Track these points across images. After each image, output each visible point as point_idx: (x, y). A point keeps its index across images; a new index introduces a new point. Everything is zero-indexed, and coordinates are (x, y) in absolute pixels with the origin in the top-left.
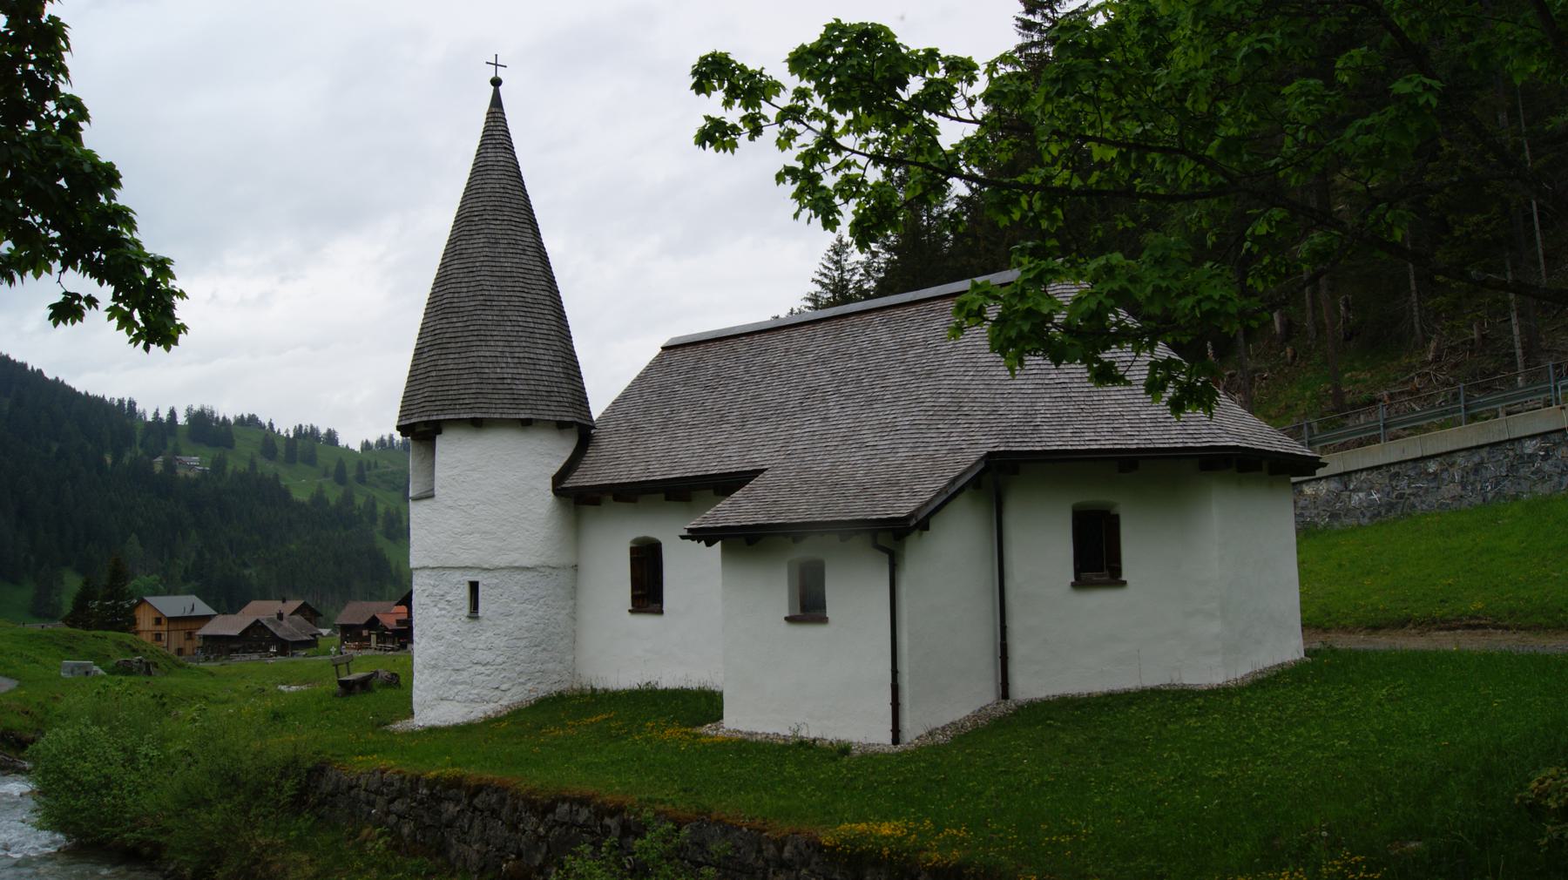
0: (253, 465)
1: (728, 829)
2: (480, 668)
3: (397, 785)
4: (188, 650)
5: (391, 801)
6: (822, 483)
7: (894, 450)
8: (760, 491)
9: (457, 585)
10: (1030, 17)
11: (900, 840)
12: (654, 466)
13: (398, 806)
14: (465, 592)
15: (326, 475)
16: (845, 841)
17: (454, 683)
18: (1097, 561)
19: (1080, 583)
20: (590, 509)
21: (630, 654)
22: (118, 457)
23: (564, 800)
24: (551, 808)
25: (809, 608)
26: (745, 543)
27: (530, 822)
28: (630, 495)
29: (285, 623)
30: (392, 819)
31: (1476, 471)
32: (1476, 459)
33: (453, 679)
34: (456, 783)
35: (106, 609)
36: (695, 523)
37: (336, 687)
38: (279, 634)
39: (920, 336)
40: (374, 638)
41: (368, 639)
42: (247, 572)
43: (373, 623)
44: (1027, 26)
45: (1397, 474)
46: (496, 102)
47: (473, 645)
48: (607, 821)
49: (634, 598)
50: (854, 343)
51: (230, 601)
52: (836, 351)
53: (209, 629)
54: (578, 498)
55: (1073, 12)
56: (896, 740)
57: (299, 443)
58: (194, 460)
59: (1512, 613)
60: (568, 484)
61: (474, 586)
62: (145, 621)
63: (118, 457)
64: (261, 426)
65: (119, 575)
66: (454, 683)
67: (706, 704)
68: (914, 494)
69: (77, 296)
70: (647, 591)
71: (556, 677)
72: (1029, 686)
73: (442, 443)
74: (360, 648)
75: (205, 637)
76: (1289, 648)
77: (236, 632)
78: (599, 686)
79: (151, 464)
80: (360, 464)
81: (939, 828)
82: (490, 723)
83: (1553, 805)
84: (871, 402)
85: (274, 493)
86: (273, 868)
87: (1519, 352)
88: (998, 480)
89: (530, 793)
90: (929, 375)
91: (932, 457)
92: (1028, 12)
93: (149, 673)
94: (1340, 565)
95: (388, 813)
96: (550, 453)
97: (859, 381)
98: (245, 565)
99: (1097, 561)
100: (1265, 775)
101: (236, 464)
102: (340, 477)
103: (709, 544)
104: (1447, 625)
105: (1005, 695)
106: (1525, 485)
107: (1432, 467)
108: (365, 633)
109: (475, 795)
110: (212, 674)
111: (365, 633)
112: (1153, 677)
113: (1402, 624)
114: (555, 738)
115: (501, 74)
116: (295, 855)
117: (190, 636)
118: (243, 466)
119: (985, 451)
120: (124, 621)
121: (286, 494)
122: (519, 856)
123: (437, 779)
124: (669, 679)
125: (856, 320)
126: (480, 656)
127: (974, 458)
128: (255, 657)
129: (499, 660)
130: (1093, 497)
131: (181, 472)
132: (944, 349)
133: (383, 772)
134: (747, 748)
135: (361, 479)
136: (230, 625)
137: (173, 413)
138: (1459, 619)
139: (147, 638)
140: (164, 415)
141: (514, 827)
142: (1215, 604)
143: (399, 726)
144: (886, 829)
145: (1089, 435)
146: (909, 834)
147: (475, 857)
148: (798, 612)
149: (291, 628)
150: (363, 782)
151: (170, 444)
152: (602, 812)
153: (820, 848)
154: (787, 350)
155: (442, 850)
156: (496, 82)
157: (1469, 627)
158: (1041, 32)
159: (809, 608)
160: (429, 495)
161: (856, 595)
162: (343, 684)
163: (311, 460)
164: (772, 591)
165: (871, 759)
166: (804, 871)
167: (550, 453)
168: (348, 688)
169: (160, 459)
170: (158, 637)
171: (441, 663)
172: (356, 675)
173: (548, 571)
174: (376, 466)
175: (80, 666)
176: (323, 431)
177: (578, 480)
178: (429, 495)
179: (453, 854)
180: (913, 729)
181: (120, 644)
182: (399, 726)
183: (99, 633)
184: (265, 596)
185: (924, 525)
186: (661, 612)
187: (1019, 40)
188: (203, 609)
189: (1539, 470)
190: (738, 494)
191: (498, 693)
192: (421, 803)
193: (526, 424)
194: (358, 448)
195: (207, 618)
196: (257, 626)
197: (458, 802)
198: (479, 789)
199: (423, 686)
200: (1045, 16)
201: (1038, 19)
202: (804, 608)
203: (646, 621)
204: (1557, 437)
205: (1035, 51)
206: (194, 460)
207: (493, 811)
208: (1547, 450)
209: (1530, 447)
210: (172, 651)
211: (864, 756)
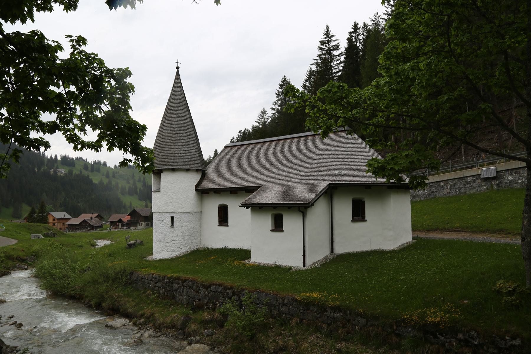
0: (81, 172)
1: (267, 294)
2: (174, 242)
3: (158, 278)
4: (63, 229)
5: (157, 283)
6: (280, 191)
7: (301, 182)
8: (261, 193)
10: (322, 46)
11: (320, 298)
12: (226, 183)
13: (158, 284)
14: (170, 219)
15: (103, 175)
16: (304, 299)
17: (166, 246)
18: (359, 214)
19: (354, 221)
21: (218, 238)
22: (39, 169)
23: (214, 285)
24: (210, 287)
25: (278, 226)
26: (257, 208)
27: (202, 291)
28: (218, 192)
29: (93, 220)
30: (157, 288)
31: (454, 185)
32: (454, 182)
33: (166, 244)
34: (178, 278)
35: (39, 217)
36: (243, 202)
37: (127, 246)
38: (91, 224)
39: (305, 147)
40: (120, 225)
41: (119, 225)
42: (79, 204)
43: (120, 221)
44: (321, 49)
45: (432, 186)
46: (178, 74)
48: (228, 291)
50: (285, 148)
51: (76, 215)
52: (279, 151)
53: (69, 222)
54: (202, 192)
55: (334, 46)
56: (304, 266)
57: (95, 165)
58: (63, 170)
60: (199, 188)
61: (172, 218)
62: (50, 220)
63: (39, 169)
64: (84, 160)
65: (43, 206)
66: (166, 246)
67: (246, 254)
68: (310, 196)
69: (127, 160)
70: (223, 220)
71: (196, 244)
72: (339, 250)
73: (163, 175)
74: (116, 228)
75: (69, 225)
76: (407, 238)
77: (78, 223)
78: (209, 247)
79: (50, 171)
80: (114, 172)
81: (330, 295)
82: (178, 258)
83: (505, 292)
84: (292, 166)
85: (88, 181)
86: (121, 303)
87: (463, 150)
88: (332, 191)
89: (203, 282)
90: (309, 159)
91: (312, 184)
92: (321, 45)
93: (54, 236)
94: (417, 212)
95: (155, 286)
96: (194, 179)
97: (288, 160)
98: (79, 202)
99: (359, 214)
100: (416, 278)
101: (76, 172)
102: (107, 176)
103: (247, 208)
104: (450, 230)
107: (442, 184)
108: (118, 224)
109: (184, 282)
110: (73, 237)
111: (118, 224)
112: (373, 248)
113: (436, 230)
114: (201, 264)
116: (127, 299)
117: (64, 224)
118: (78, 172)
119: (328, 183)
120: (44, 220)
121: (91, 181)
122: (199, 300)
123: (171, 277)
124: (231, 245)
125: (285, 141)
126: (174, 238)
127: (326, 185)
128: (84, 230)
129: (180, 239)
130: (357, 196)
131: (59, 174)
132: (313, 151)
133: (153, 274)
134: (260, 268)
135: (114, 176)
136: (76, 221)
137: (56, 156)
139: (51, 225)
140: (53, 157)
141: (197, 292)
142: (390, 226)
143: (149, 258)
144: (315, 295)
145: (358, 179)
146: (322, 297)
147: (185, 300)
148: (274, 229)
149: (95, 222)
150: (146, 277)
151: (55, 165)
152: (226, 288)
153: (296, 300)
154: (264, 149)
155: (174, 298)
156: (178, 68)
157: (455, 231)
158: (325, 51)
159: (278, 226)
160: (158, 190)
161: (292, 223)
162: (129, 245)
163: (98, 170)
164: (266, 221)
165: (298, 272)
166: (291, 307)
167: (194, 179)
168: (130, 246)
169: (52, 170)
170: (54, 224)
172: (132, 242)
174: (118, 173)
175: (37, 236)
176: (102, 162)
177: (202, 187)
178: (158, 190)
179: (177, 299)
180: (309, 262)
181: (45, 228)
183: (38, 224)
184: (85, 213)
185: (313, 205)
186: (228, 226)
187: (319, 53)
188: (69, 217)
189: (472, 186)
190: (255, 193)
192: (166, 284)
193: (188, 170)
194: (113, 167)
195: (69, 219)
196: (84, 221)
197: (178, 284)
198: (185, 280)
200: (326, 46)
201: (324, 47)
202: (276, 227)
204: (477, 177)
205: (324, 56)
206: (63, 170)
207: (190, 287)
208: (474, 180)
209: (469, 179)
210: (58, 229)
211: (296, 271)
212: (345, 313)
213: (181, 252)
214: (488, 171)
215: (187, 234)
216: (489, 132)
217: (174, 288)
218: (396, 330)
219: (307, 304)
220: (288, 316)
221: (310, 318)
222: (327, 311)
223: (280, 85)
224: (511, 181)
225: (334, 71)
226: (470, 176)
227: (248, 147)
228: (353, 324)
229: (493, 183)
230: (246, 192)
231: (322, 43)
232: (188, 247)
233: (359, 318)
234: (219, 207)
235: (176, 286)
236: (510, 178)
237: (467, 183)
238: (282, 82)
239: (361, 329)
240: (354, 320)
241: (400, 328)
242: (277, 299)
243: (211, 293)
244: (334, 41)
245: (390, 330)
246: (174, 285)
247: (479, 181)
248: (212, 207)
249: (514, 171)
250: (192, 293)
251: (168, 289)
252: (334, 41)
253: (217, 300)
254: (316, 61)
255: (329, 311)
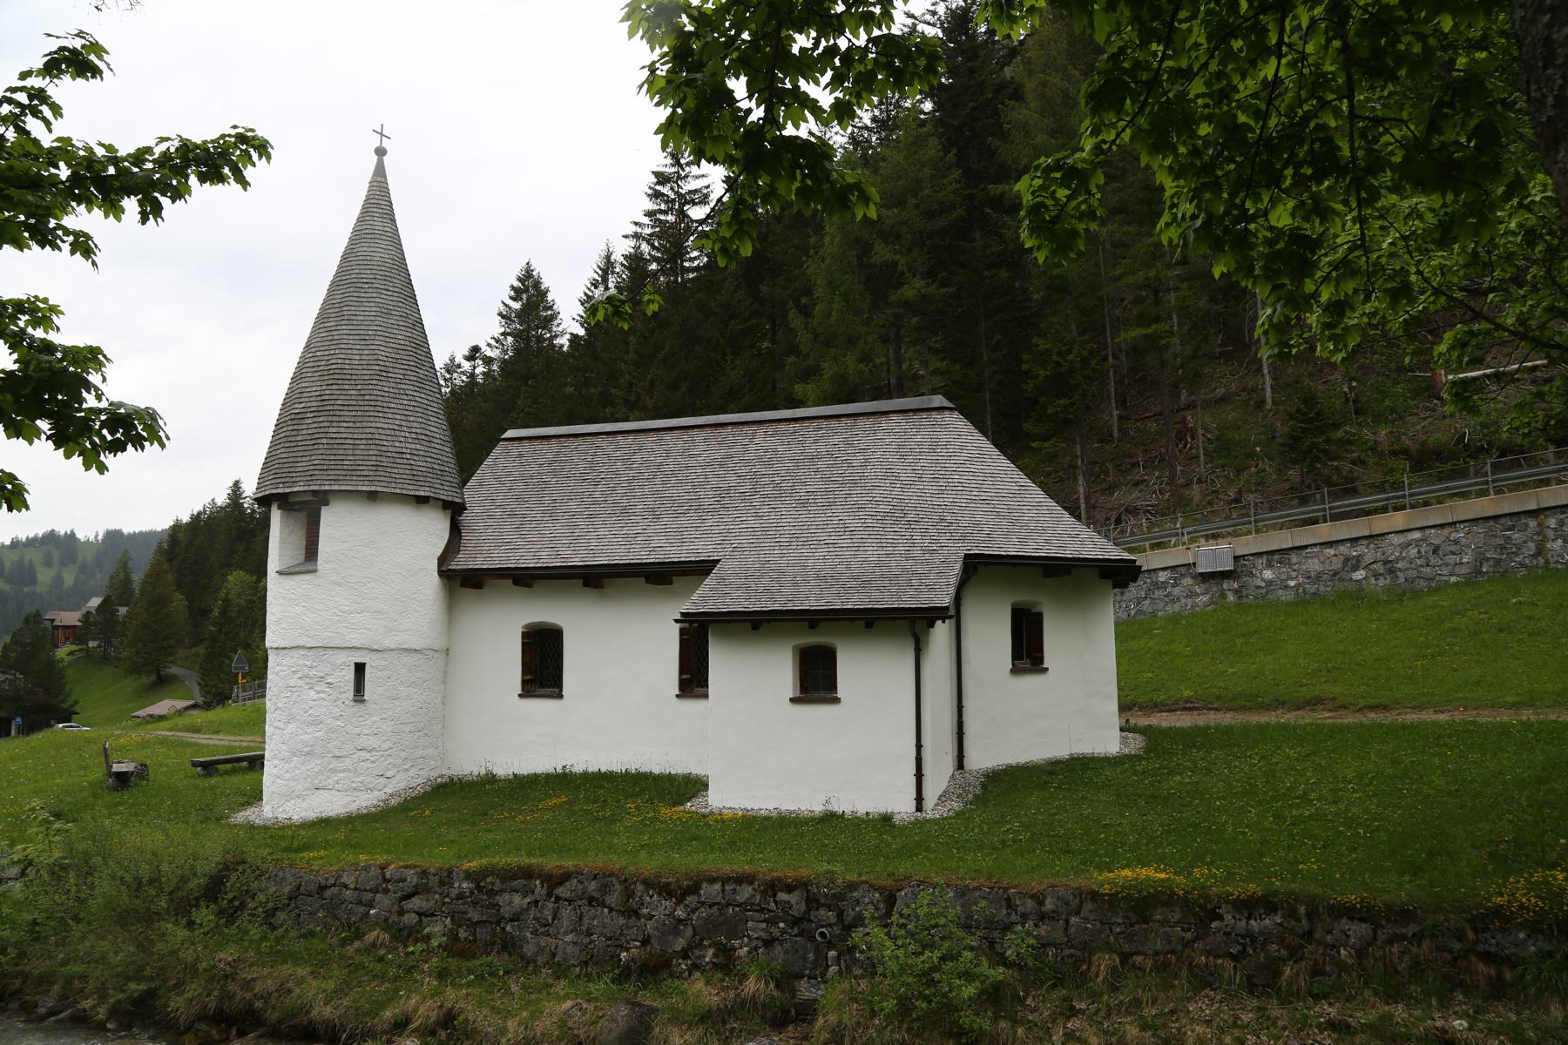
2: (363, 754)
9: (340, 667)
14: (350, 674)
16: (1124, 887)
17: (334, 771)
19: (1015, 671)
20: (470, 592)
21: (524, 740)
23: (712, 880)
24: (694, 889)
25: (817, 681)
27: (660, 908)
28: (525, 579)
46: (380, 171)
47: (358, 730)
48: (782, 896)
49: (524, 682)
54: (462, 581)
55: (696, 191)
56: (919, 808)
59: (1218, 698)
61: (360, 669)
66: (334, 771)
67: (695, 786)
72: (981, 758)
89: (658, 875)
92: (659, 183)
105: (960, 765)
106: (1160, 605)
109: (560, 883)
115: (386, 144)
122: (646, 942)
124: (585, 759)
129: (385, 746)
130: (1024, 597)
138: (1176, 702)
143: (241, 816)
155: (509, 946)
156: (381, 152)
157: (1186, 709)
158: (666, 202)
159: (817, 681)
161: (869, 673)
166: (1074, 920)
168: (122, 779)
171: (318, 750)
173: (431, 653)
177: (462, 562)
179: (529, 949)
182: (241, 816)
186: (560, 696)
187: (651, 206)
191: (382, 780)
199: (272, 776)
203: (540, 707)
204: (1183, 570)
209: (1163, 576)
212: (1292, 914)
213: (389, 790)
214: (1214, 554)
215: (408, 728)
216: (1133, 465)
217: (506, 911)
218: (1477, 942)
219: (1140, 905)
220: (1067, 952)
221: (1159, 946)
222: (1221, 918)
223: (513, 288)
224: (1270, 582)
225: (687, 264)
226: (1164, 569)
227: (598, 441)
228: (1326, 945)
229: (1225, 586)
230: (587, 584)
231: (662, 178)
232: (413, 772)
233: (1345, 923)
234: (524, 635)
235: (518, 901)
236: (1268, 574)
237: (1158, 586)
238: (519, 279)
239: (1360, 954)
240: (1329, 932)
241: (1487, 935)
242: (1008, 900)
243: (704, 912)
244: (697, 177)
245: (1457, 945)
246: (502, 899)
247: (1187, 581)
248: (498, 633)
249: (1276, 557)
250: (603, 920)
251: (474, 915)
252: (697, 177)
253: (732, 935)
254: (635, 228)
255: (1228, 917)
